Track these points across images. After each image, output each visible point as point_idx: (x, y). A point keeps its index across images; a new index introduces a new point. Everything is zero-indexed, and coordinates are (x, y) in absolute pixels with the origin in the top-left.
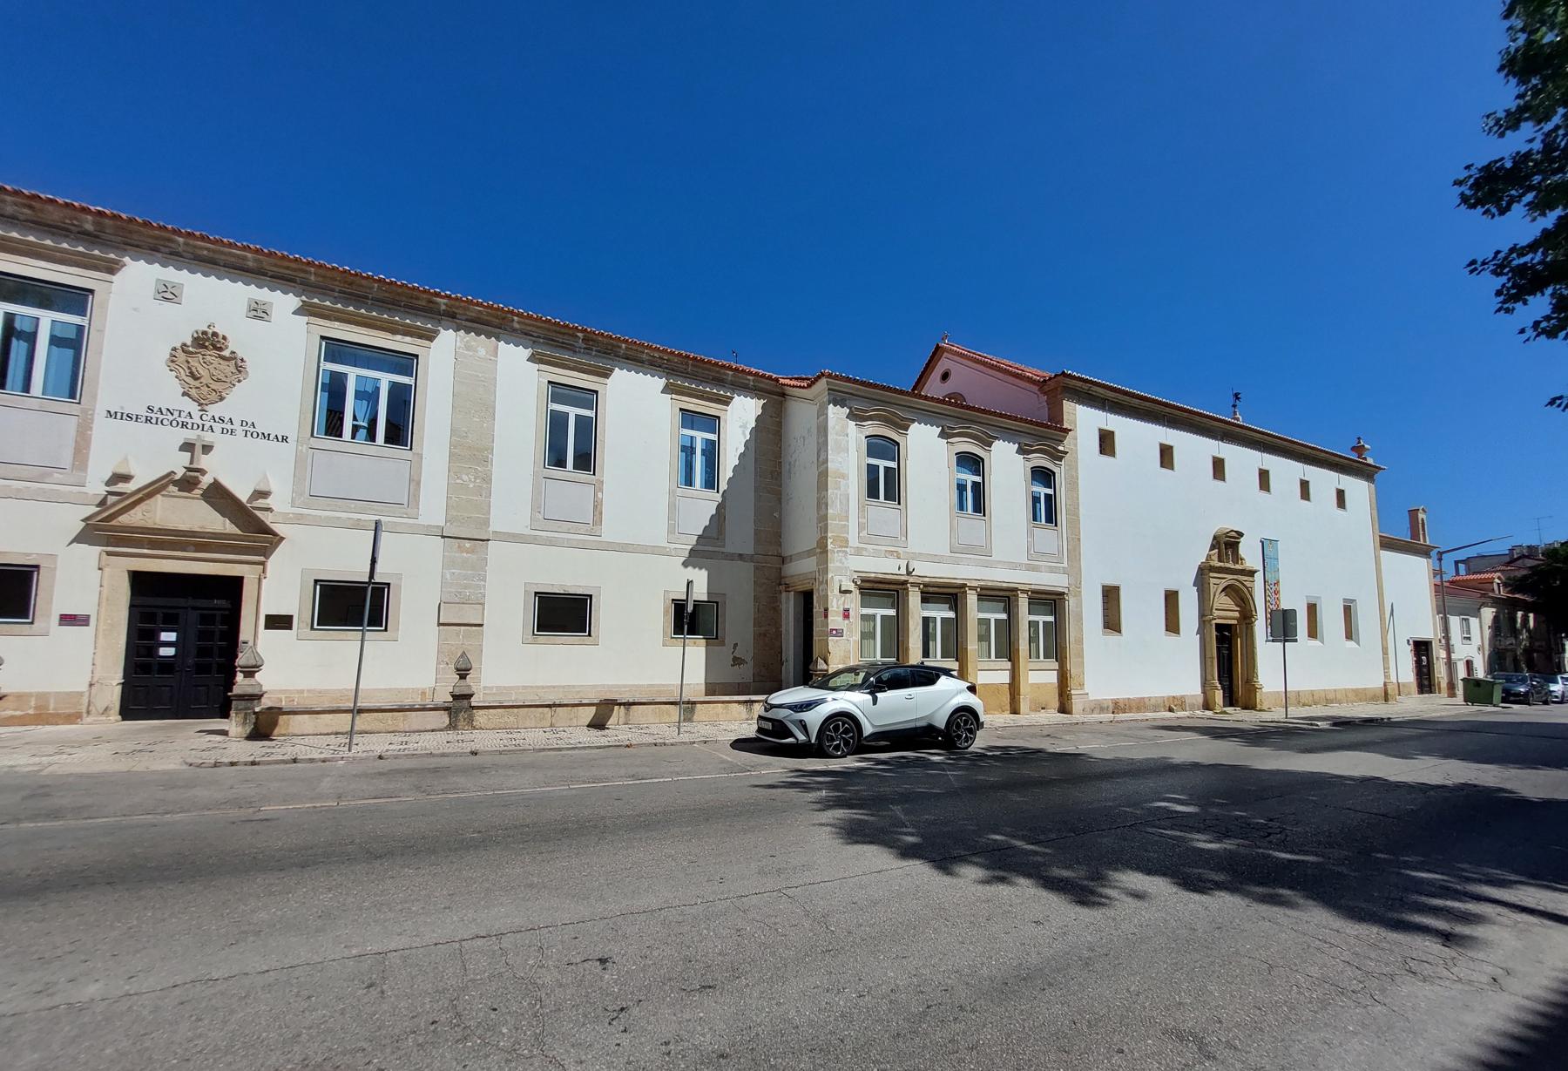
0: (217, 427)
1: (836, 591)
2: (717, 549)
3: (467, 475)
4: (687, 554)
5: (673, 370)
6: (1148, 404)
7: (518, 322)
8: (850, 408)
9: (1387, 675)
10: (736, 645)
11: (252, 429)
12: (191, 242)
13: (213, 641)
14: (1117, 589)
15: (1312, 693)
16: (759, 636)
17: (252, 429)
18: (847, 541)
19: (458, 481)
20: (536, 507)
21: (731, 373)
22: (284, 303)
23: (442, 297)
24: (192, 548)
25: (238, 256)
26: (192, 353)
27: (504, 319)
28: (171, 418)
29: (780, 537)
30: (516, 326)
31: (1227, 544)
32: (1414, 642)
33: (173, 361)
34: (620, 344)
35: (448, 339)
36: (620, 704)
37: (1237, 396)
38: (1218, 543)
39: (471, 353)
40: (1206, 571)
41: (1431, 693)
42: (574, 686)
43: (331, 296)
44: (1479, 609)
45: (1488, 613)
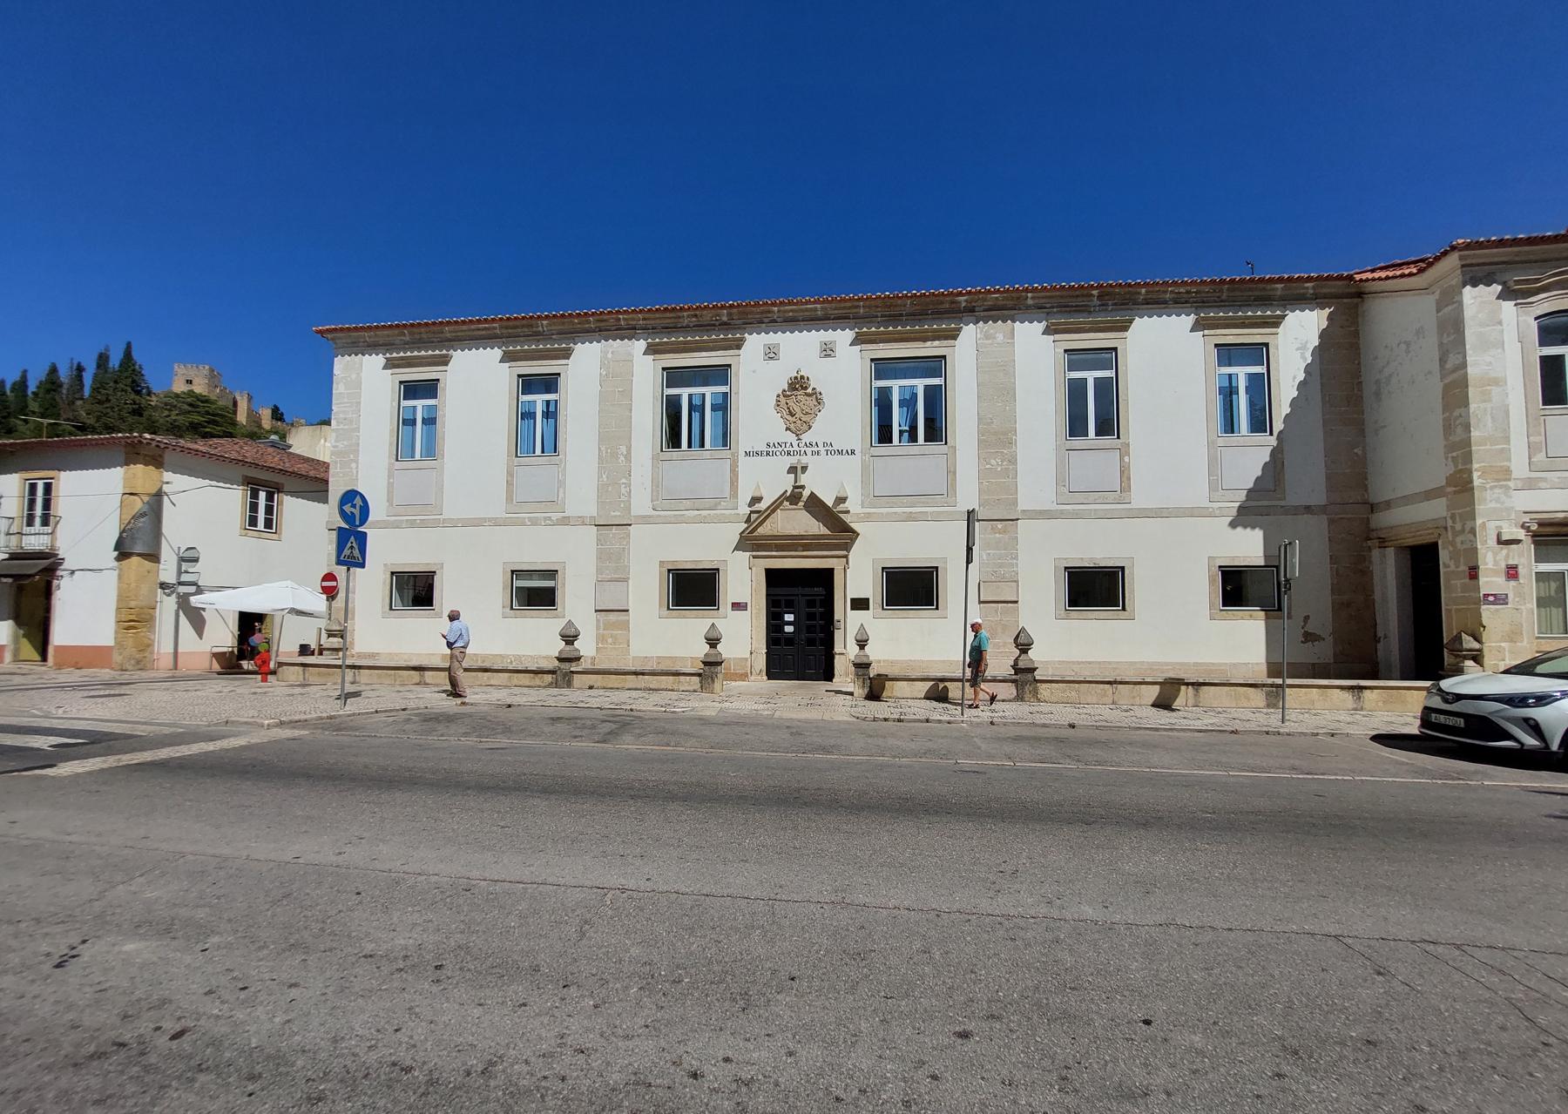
0: (809, 450)
1: (1492, 542)
2: (1274, 503)
3: (995, 459)
4: (1234, 512)
5: (1203, 302)
8: (1504, 284)
10: (1307, 618)
11: (830, 448)
12: (782, 308)
13: (815, 620)
16: (1339, 607)
17: (830, 448)
18: (1508, 471)
19: (988, 466)
20: (1061, 480)
22: (843, 337)
23: (963, 295)
24: (801, 548)
25: (811, 310)
26: (789, 396)
27: (1018, 298)
28: (780, 449)
29: (1366, 479)
30: (1030, 302)
33: (778, 405)
34: (1138, 290)
36: (1187, 684)
39: (990, 341)
42: (1110, 663)
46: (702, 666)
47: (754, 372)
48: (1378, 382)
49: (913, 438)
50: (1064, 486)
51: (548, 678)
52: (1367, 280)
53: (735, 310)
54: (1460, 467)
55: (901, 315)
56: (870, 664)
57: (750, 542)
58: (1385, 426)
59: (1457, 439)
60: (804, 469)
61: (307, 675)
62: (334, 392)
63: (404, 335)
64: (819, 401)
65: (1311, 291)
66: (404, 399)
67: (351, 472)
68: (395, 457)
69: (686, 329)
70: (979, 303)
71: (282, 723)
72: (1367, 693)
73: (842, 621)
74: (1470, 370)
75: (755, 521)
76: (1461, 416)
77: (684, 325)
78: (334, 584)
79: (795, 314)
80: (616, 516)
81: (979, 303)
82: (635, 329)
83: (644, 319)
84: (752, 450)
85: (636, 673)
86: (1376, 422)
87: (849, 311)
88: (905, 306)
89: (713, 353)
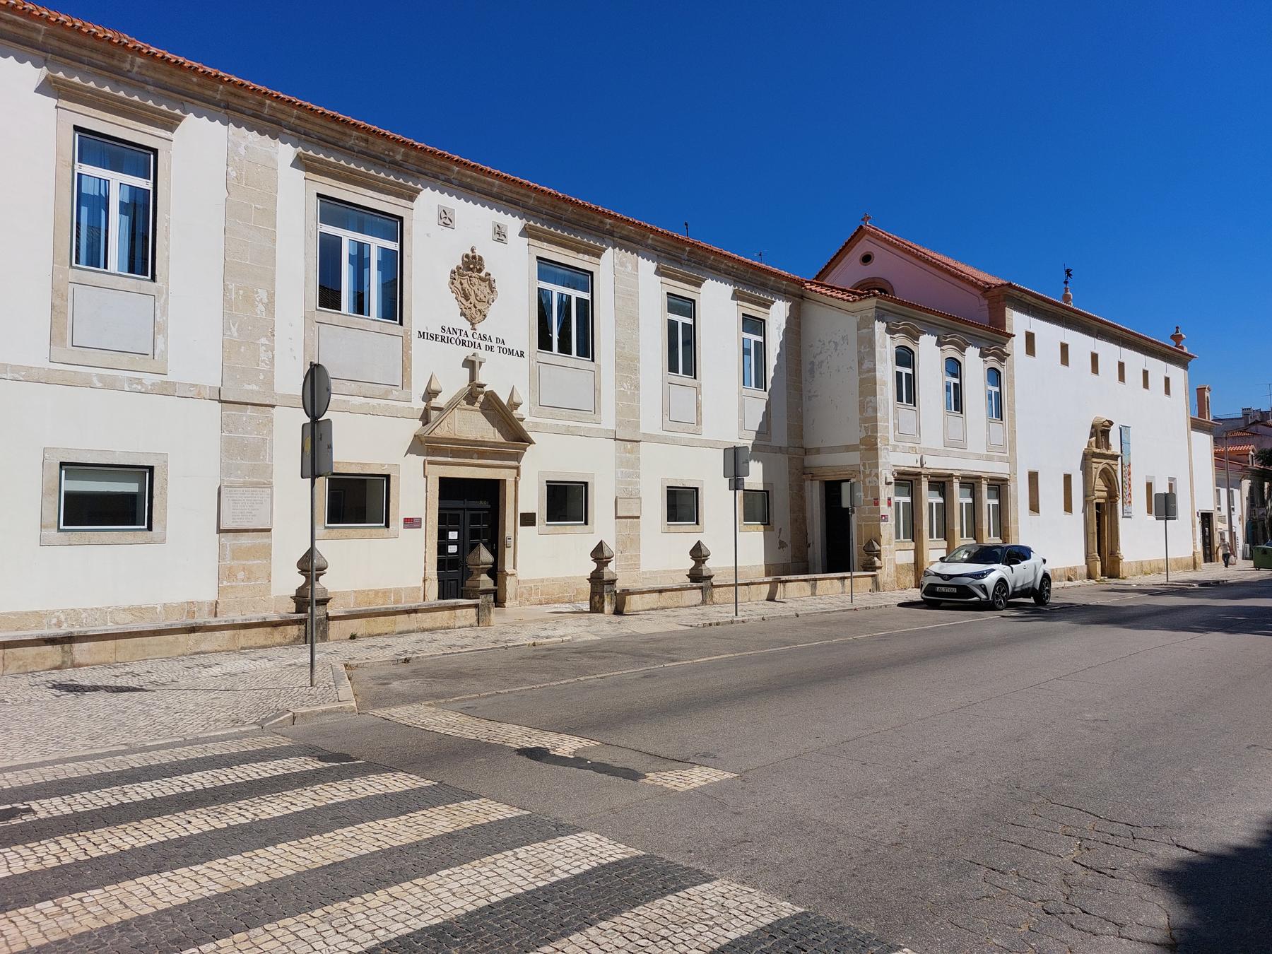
0: (483, 343)
6: (1055, 308)
7: (652, 239)
9: (1195, 547)
11: (502, 346)
12: (463, 171)
14: (1070, 476)
15: (1150, 563)
20: (666, 410)
21: (43, 28)
22: (514, 224)
24: (475, 455)
25: (489, 183)
31: (1101, 432)
32: (1202, 514)
35: (611, 255)
37: (1068, 272)
38: (1096, 431)
39: (623, 269)
40: (1089, 457)
41: (1211, 561)
43: (540, 218)
44: (1241, 481)
45: (1246, 484)
48: (812, 363)
51: (293, 631)
53: (414, 153)
54: (869, 434)
57: (424, 446)
58: (817, 396)
64: (492, 289)
69: (349, 152)
70: (618, 230)
73: (513, 538)
80: (252, 392)
81: (618, 230)
83: (298, 118)
84: (426, 331)
85: (408, 612)
86: (810, 392)
87: (520, 198)
88: (567, 211)
89: (382, 196)
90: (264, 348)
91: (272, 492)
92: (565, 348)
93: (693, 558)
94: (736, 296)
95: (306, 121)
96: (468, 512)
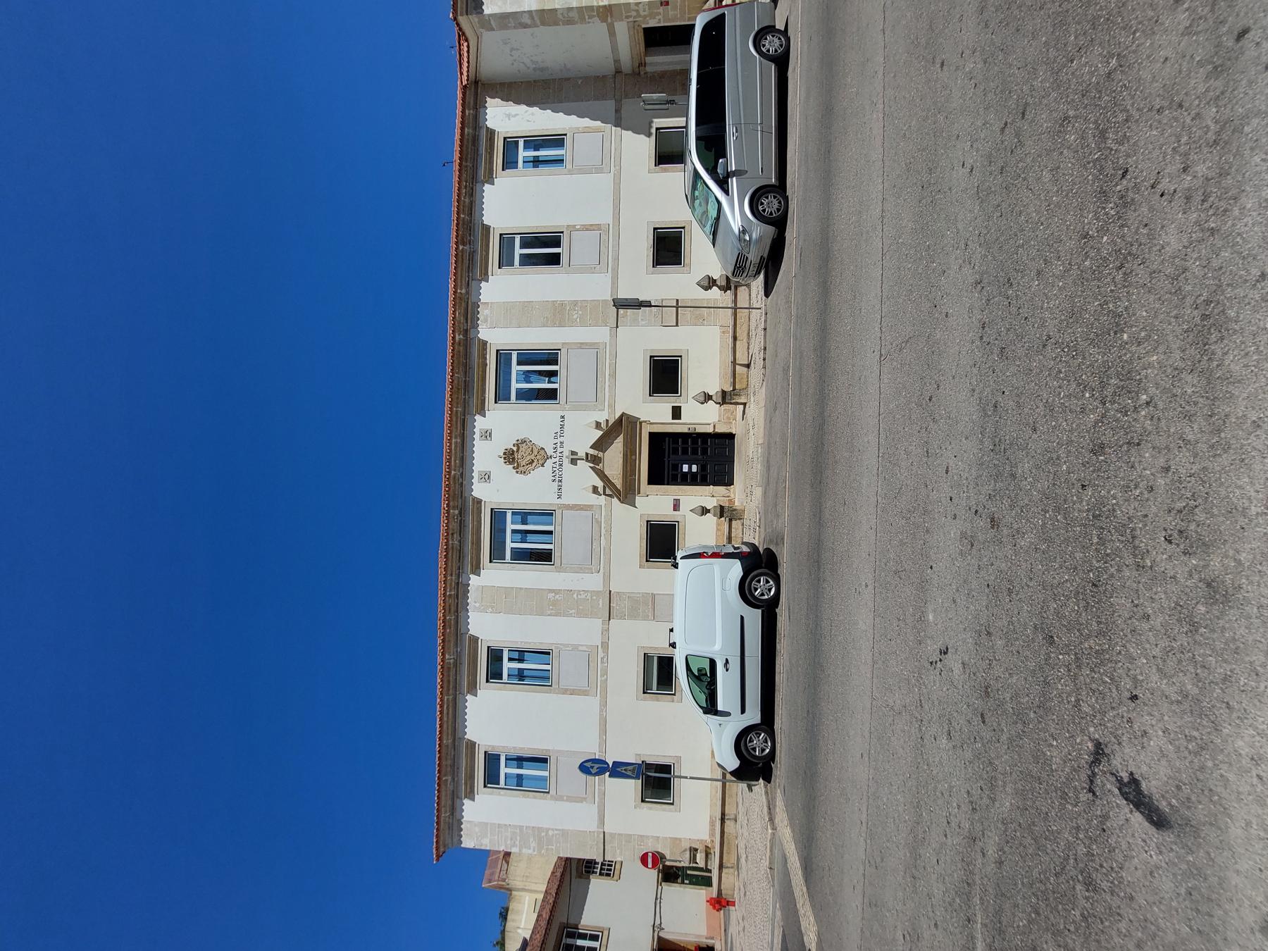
0: (559, 450)
4: (619, 129)
5: (473, 178)
7: (461, 290)
12: (453, 467)
20: (592, 270)
22: (480, 423)
25: (456, 446)
30: (464, 291)
33: (525, 472)
39: (489, 319)
46: (723, 519)
47: (498, 491)
48: (534, 69)
49: (553, 374)
50: (595, 268)
52: (468, 76)
53: (451, 504)
54: (595, 14)
55: (465, 381)
56: (721, 506)
57: (627, 494)
58: (565, 65)
59: (577, 15)
60: (573, 453)
61: (729, 865)
62: (488, 848)
63: (446, 780)
64: (524, 442)
65: (472, 112)
66: (499, 784)
67: (556, 834)
68: (546, 794)
71: (771, 820)
72: (733, 877)
73: (689, 426)
74: (534, 8)
75: (612, 491)
76: (562, 14)
77: (459, 544)
78: (650, 854)
79: (458, 459)
80: (603, 604)
82: (458, 583)
83: (451, 575)
90: (579, 596)
91: (658, 594)
92: (555, 362)
93: (710, 288)
94: (471, 795)
95: (452, 572)
96: (671, 456)
